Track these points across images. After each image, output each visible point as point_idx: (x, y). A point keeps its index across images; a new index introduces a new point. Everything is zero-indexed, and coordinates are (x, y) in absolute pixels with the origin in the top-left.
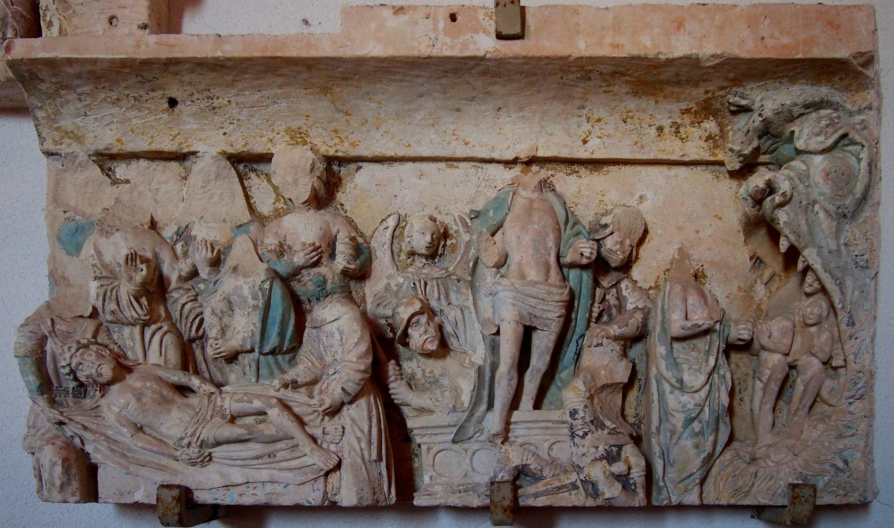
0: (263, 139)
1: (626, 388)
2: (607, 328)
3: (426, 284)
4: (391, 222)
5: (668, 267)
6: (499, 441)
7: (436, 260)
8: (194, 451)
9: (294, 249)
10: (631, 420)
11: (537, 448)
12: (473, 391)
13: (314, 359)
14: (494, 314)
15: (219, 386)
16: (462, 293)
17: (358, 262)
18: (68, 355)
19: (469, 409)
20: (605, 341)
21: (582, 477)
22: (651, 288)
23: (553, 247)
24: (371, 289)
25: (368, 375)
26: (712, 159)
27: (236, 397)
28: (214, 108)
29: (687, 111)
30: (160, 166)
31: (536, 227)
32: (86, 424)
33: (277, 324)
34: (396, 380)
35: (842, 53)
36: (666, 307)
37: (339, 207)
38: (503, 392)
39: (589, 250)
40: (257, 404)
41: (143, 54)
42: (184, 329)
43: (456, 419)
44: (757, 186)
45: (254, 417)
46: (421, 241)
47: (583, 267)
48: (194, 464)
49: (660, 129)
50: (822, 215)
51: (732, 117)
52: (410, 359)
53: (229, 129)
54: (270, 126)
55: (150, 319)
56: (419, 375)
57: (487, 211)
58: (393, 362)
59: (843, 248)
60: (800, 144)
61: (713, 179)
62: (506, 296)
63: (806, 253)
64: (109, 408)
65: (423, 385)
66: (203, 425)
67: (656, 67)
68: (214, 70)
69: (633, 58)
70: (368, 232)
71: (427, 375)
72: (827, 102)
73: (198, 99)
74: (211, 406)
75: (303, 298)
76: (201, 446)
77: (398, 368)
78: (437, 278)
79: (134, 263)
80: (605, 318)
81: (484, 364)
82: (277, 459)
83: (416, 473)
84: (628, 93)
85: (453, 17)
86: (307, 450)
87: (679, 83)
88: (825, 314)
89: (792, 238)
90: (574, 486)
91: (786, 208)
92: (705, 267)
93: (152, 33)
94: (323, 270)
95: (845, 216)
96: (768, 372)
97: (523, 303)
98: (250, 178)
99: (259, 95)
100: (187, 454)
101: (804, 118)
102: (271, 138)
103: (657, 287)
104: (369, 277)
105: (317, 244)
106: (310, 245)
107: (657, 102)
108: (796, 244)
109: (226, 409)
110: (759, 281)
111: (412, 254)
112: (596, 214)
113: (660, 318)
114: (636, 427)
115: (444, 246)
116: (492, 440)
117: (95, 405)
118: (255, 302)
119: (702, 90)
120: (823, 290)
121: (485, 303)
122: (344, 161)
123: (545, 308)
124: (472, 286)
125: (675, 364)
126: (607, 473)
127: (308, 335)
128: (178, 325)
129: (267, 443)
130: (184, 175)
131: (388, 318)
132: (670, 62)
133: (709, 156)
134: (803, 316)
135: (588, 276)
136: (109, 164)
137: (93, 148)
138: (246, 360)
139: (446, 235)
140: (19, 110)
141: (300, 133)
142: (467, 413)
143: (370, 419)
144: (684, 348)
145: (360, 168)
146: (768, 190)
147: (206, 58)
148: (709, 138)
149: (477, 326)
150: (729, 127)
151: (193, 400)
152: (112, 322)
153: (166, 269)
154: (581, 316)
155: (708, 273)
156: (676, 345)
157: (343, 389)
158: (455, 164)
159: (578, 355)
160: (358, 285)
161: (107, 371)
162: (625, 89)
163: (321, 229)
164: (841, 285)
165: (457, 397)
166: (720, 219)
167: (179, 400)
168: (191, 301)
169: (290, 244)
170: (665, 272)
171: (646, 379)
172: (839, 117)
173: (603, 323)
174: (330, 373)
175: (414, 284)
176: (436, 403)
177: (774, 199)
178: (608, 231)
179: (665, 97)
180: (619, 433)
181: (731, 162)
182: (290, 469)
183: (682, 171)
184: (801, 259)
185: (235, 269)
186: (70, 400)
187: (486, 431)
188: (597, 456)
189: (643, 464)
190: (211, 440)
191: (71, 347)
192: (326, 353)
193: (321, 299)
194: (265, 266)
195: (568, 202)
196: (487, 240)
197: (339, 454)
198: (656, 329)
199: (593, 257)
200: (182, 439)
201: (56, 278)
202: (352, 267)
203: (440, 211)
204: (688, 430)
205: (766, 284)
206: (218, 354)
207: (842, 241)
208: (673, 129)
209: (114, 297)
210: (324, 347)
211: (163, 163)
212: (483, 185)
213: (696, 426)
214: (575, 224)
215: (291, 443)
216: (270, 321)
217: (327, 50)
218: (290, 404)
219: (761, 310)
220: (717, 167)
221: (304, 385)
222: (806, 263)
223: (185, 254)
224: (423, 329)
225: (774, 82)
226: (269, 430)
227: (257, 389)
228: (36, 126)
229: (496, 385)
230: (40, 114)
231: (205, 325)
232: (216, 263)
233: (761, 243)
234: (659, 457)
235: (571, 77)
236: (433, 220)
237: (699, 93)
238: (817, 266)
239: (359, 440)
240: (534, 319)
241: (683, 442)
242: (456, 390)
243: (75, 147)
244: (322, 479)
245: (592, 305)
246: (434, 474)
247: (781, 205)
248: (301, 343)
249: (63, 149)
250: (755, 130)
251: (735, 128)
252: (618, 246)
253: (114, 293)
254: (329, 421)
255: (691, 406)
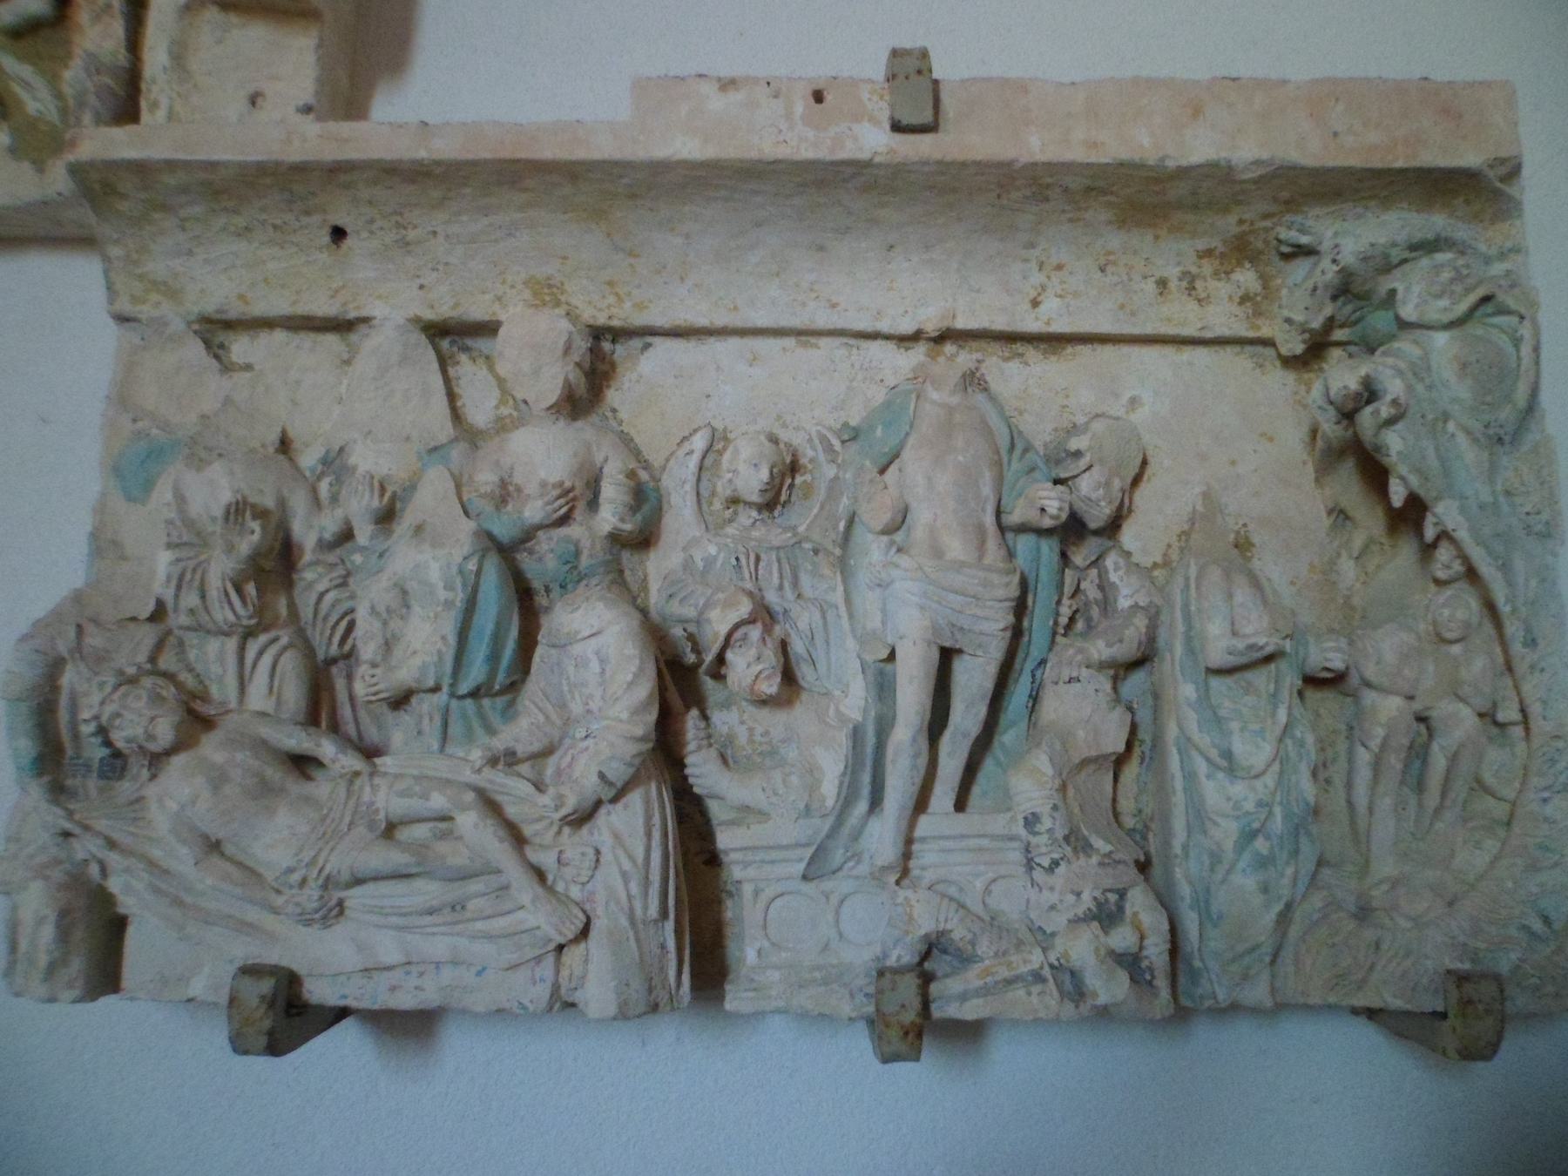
0: (487, 297)
1: (1120, 761)
2: (1086, 645)
3: (758, 559)
4: (699, 443)
5: (1186, 527)
6: (893, 878)
7: (776, 513)
8: (312, 894)
9: (527, 491)
10: (1129, 822)
11: (961, 890)
12: (844, 774)
13: (550, 707)
14: (884, 623)
15: (370, 753)
16: (822, 576)
17: (639, 517)
18: (96, 698)
19: (836, 813)
20: (1085, 672)
21: (1053, 959)
22: (1155, 565)
23: (992, 497)
24: (658, 566)
25: (650, 745)
26: (1251, 334)
27: (401, 785)
28: (408, 244)
29: (1208, 253)
30: (307, 339)
31: (960, 458)
32: (116, 836)
33: (486, 640)
34: (699, 748)
35: (1470, 158)
36: (1193, 608)
37: (609, 414)
38: (899, 787)
39: (1056, 504)
40: (438, 802)
41: (295, 154)
42: (318, 638)
43: (810, 832)
44: (1345, 387)
45: (431, 825)
46: (752, 479)
47: (1049, 532)
48: (308, 923)
49: (1162, 283)
50: (1461, 438)
51: (1282, 263)
52: (726, 705)
53: (429, 278)
54: (500, 274)
55: (258, 624)
56: (742, 738)
57: (872, 428)
58: (694, 713)
59: (1501, 499)
60: (1408, 312)
61: (1254, 369)
62: (906, 589)
63: (1440, 508)
64: (160, 800)
65: (748, 758)
66: (332, 843)
67: (1157, 180)
68: (413, 182)
69: (1121, 164)
70: (656, 460)
71: (758, 738)
72: (1446, 240)
73: (382, 228)
74: (352, 803)
75: (537, 584)
76: (325, 887)
77: (703, 724)
78: (778, 548)
79: (240, 520)
80: (1080, 625)
81: (864, 719)
82: (468, 915)
83: (729, 931)
84: (1110, 222)
85: (818, 97)
86: (526, 898)
87: (1195, 207)
88: (1475, 620)
89: (1414, 481)
90: (1038, 977)
91: (1399, 426)
92: (1251, 527)
93: (319, 119)
94: (574, 531)
95: (1500, 440)
96: (1380, 732)
97: (940, 603)
98: (458, 363)
99: (486, 221)
100: (298, 904)
101: (1407, 267)
102: (500, 293)
103: (1166, 563)
104: (656, 542)
105: (568, 484)
106: (554, 486)
107: (1157, 237)
108: (1422, 493)
109: (377, 810)
110: (1344, 553)
111: (734, 501)
112: (1056, 430)
113: (1180, 627)
114: (1138, 837)
115: (791, 486)
116: (878, 875)
117: (136, 795)
118: (450, 595)
119: (1232, 219)
120: (1471, 574)
121: (868, 601)
122: (619, 334)
123: (979, 612)
124: (843, 566)
125: (1216, 721)
126: (1103, 952)
127: (542, 657)
128: (309, 632)
129: (449, 880)
130: (346, 356)
131: (686, 621)
132: (1183, 172)
133: (1247, 330)
134: (1435, 623)
135: (1051, 549)
136: (221, 337)
137: (196, 310)
138: (425, 705)
139: (794, 468)
140: (84, 241)
141: (550, 286)
142: (829, 822)
143: (649, 835)
144: (1230, 688)
145: (647, 346)
146: (1366, 395)
147: (401, 161)
148: (1245, 299)
149: (851, 644)
150: (1279, 281)
151: (321, 788)
152: (188, 628)
153: (297, 528)
154: (1038, 624)
155: (1256, 539)
156: (1215, 682)
157: (602, 776)
158: (813, 340)
159: (1035, 698)
160: (636, 557)
161: (165, 732)
162: (1104, 216)
163: (575, 455)
164: (1505, 568)
165: (813, 788)
166: (1271, 440)
167: (296, 787)
168: (337, 586)
169: (519, 482)
170: (1179, 536)
171: (1153, 740)
172: (1468, 266)
173: (1076, 635)
174: (578, 736)
175: (737, 559)
176: (774, 799)
177: (1377, 412)
178: (1083, 463)
179: (1170, 231)
180: (1119, 862)
181: (1287, 341)
182: (490, 937)
183: (1201, 353)
184: (1430, 520)
185: (419, 529)
186: (93, 783)
187: (866, 856)
188: (1080, 911)
189: (1166, 926)
190: (345, 876)
191: (104, 683)
192: (573, 698)
193: (569, 586)
194: (470, 525)
195: (1007, 408)
196: (871, 481)
197: (587, 907)
198: (1174, 651)
199: (1064, 516)
200: (290, 870)
201: (104, 544)
202: (628, 527)
203: (784, 422)
204: (1247, 857)
205: (1357, 558)
206: (375, 694)
207: (1499, 488)
208: (1184, 284)
209: (196, 583)
210: (569, 684)
211: (312, 335)
212: (860, 377)
213: (1261, 845)
214: (1026, 450)
215: (494, 881)
216: (472, 634)
217: (603, 148)
218: (499, 798)
219: (1352, 608)
220: (1260, 349)
221: (528, 759)
222: (1439, 528)
223: (334, 499)
224: (753, 652)
225: (1355, 207)
226: (457, 857)
227: (439, 767)
228: (106, 272)
229: (889, 768)
230: (115, 251)
231: (358, 632)
232: (386, 517)
233: (1347, 485)
234: (1192, 908)
235: (1015, 195)
236: (774, 440)
237: (1229, 224)
238: (1462, 535)
239: (625, 876)
240: (958, 636)
241: (1237, 879)
242: (812, 773)
243: (167, 309)
244: (550, 959)
245: (1059, 602)
246: (766, 944)
247: (1391, 422)
248: (526, 671)
249: (145, 311)
250: (1326, 287)
251: (1290, 281)
252: (1101, 491)
253: (198, 577)
254: (570, 836)
255: (1249, 806)
